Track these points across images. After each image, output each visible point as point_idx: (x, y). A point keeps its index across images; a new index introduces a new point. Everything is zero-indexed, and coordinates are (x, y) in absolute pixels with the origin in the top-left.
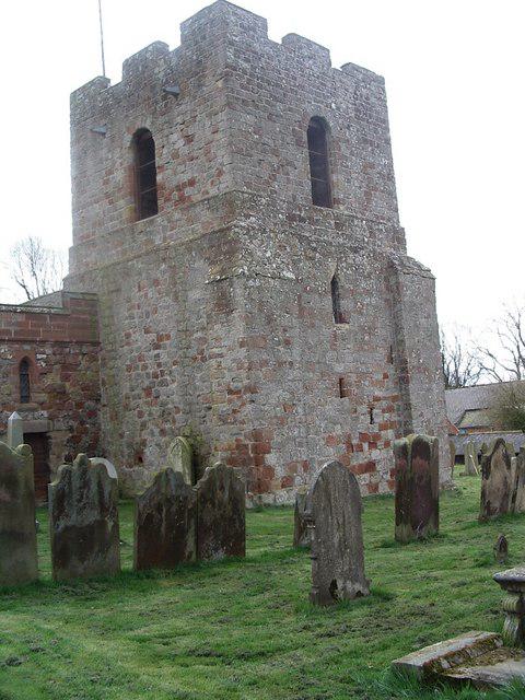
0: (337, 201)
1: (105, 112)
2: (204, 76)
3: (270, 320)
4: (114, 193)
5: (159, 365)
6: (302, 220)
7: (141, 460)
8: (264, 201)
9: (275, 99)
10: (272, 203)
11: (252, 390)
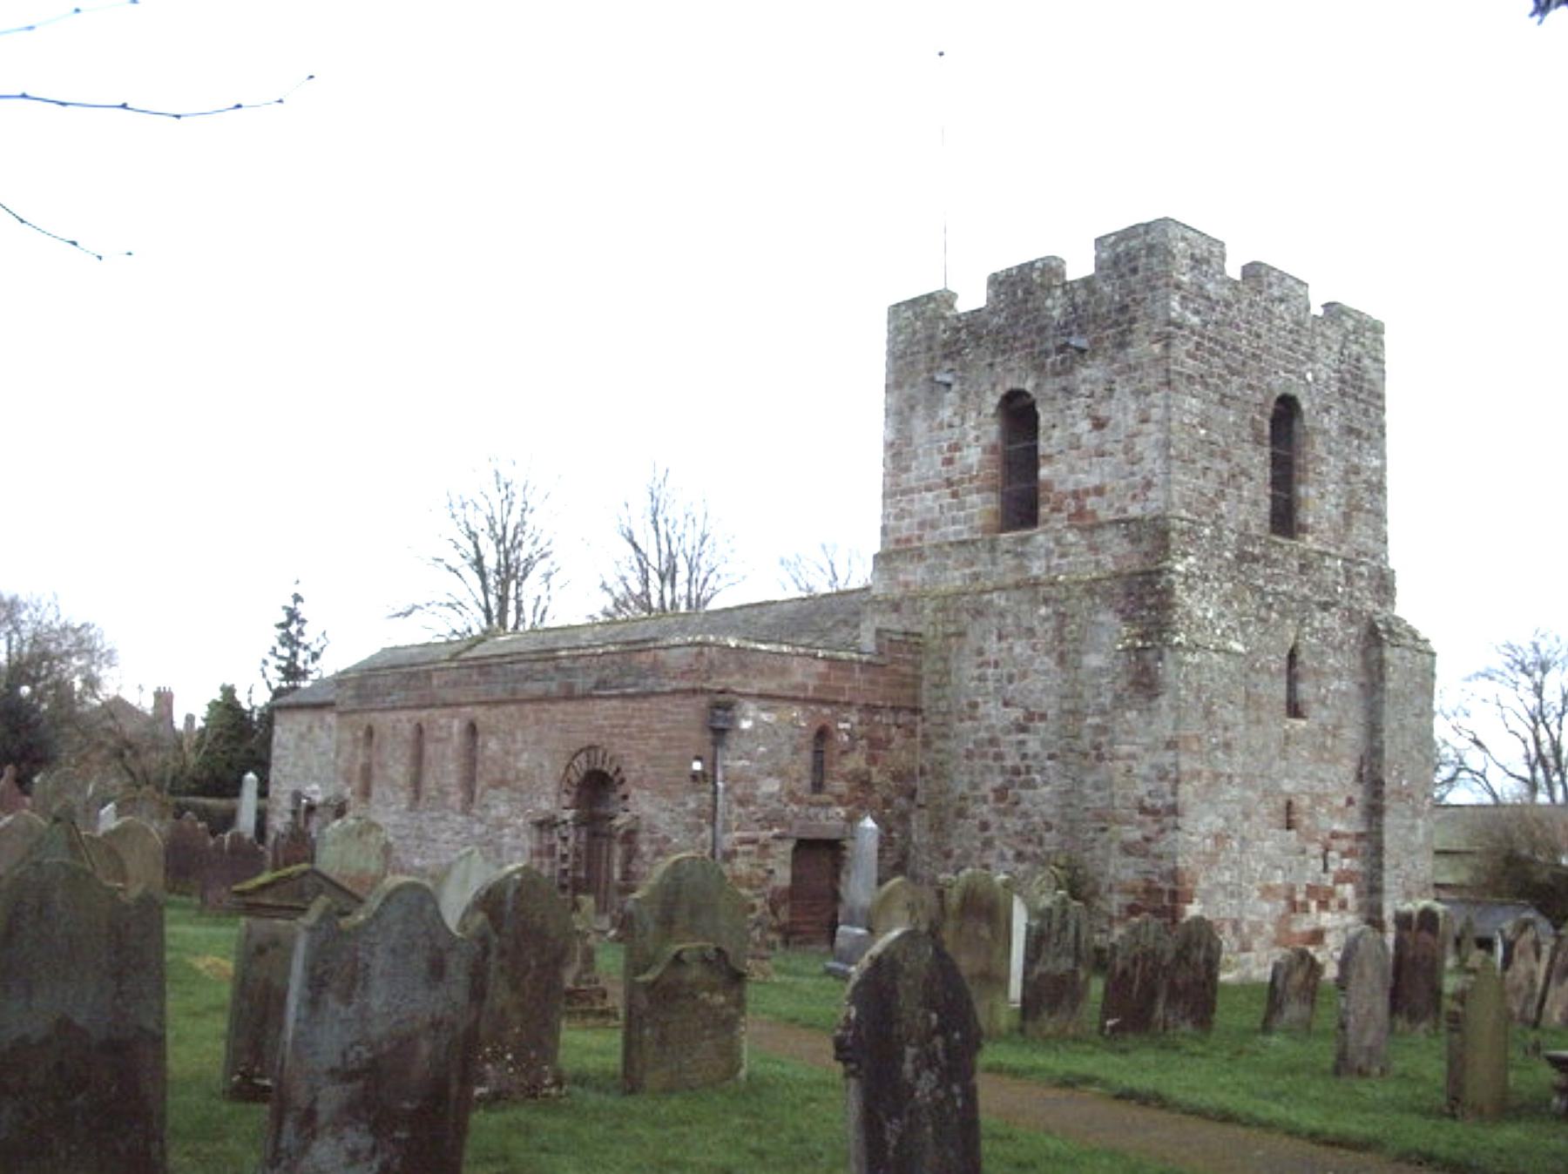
0: (1304, 529)
1: (952, 351)
3: (1208, 712)
4: (962, 481)
5: (1024, 756)
6: (1255, 559)
8: (1207, 531)
10: (1217, 536)
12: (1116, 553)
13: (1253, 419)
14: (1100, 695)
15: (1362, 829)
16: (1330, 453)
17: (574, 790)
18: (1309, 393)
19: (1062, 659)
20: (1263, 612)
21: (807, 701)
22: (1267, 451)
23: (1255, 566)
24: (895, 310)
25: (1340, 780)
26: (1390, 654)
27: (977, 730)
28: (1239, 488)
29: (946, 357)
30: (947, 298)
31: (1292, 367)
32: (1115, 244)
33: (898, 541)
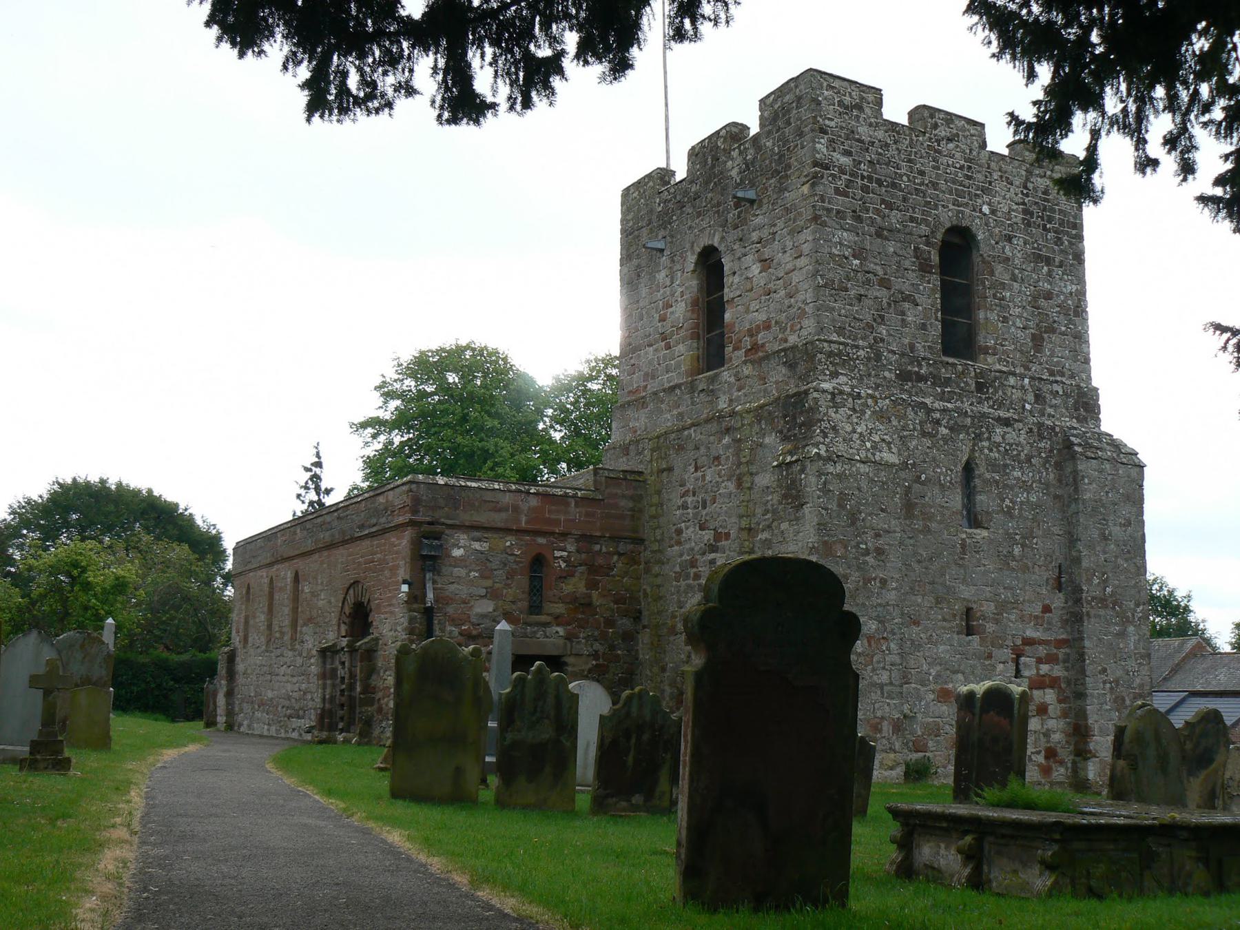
1: (664, 220)
2: (787, 177)
3: (853, 518)
4: (672, 334)
6: (921, 378)
9: (890, 206)
20: (929, 428)
21: (520, 532)
22: (935, 279)
25: (1034, 589)
27: (681, 555)
28: (903, 313)
32: (775, 100)
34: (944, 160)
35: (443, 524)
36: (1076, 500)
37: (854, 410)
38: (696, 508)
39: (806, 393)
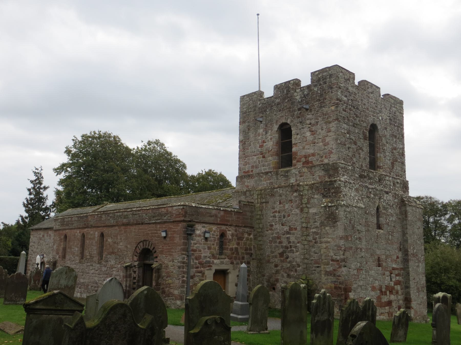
0: (379, 167)
1: (263, 110)
3: (353, 227)
6: (365, 177)
7: (274, 289)
10: (353, 170)
11: (344, 260)
12: (319, 175)
13: (363, 131)
14: (316, 222)
15: (402, 267)
16: (387, 143)
17: (138, 255)
18: (380, 123)
19: (302, 210)
23: (365, 179)
24: (242, 98)
25: (395, 251)
26: (409, 209)
27: (273, 234)
28: (360, 154)
29: (260, 113)
30: (260, 93)
31: (375, 115)
32: (319, 74)
33: (244, 172)
34: (370, 100)
35: (194, 221)
36: (406, 220)
37: (350, 188)
38: (280, 217)
39: (335, 181)
